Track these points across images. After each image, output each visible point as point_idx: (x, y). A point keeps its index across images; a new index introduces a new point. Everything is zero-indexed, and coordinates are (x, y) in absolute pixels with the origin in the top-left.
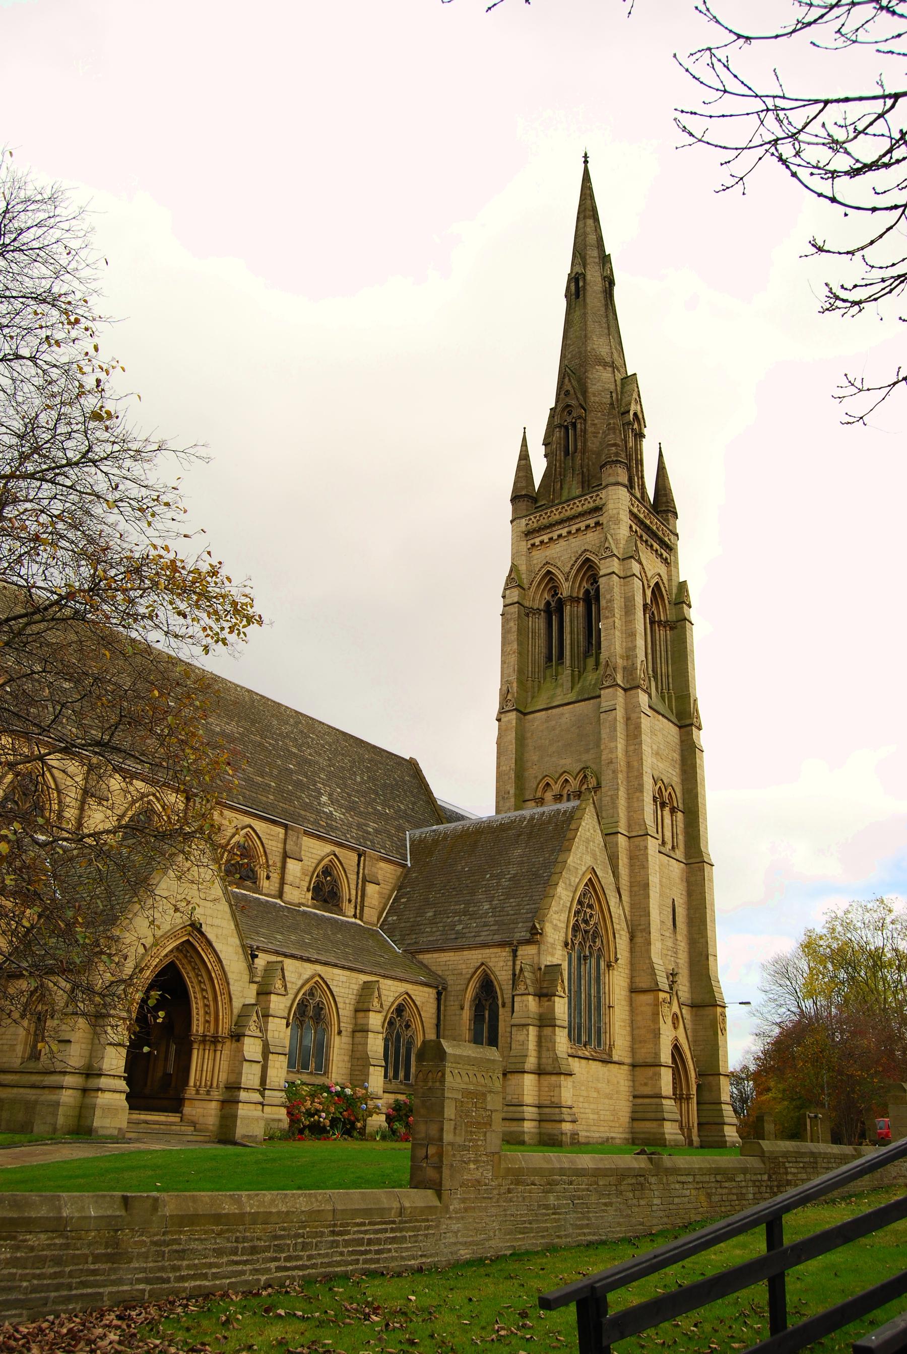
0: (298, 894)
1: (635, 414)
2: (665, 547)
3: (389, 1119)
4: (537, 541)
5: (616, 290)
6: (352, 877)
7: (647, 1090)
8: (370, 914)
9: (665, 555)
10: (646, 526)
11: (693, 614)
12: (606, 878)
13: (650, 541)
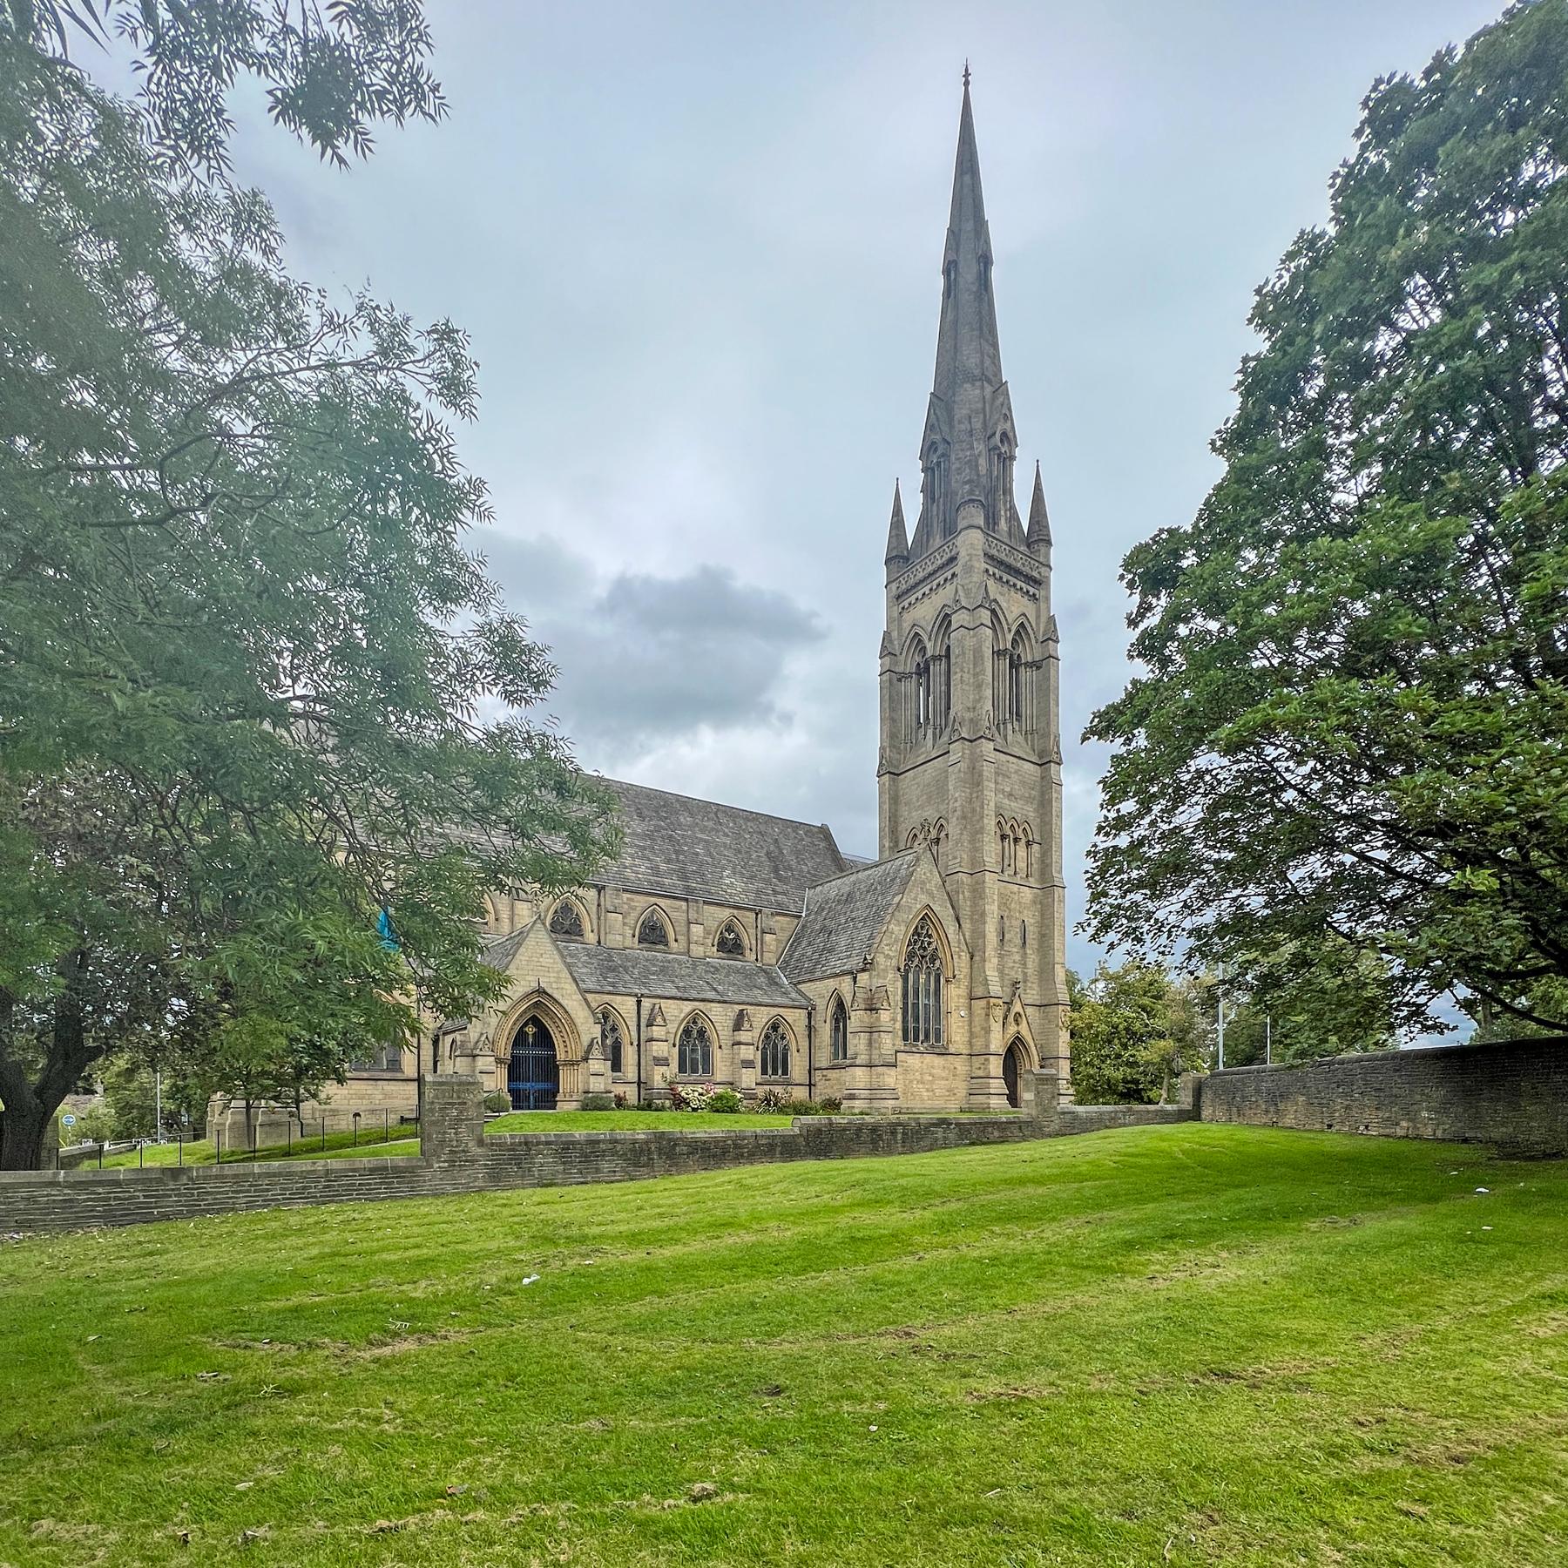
0: (705, 948)
1: (1004, 434)
2: (1034, 583)
3: (1450, 985)
4: (906, 604)
5: (995, 274)
6: (752, 931)
7: (980, 1073)
8: (769, 958)
9: (1032, 591)
10: (1001, 563)
11: (1061, 649)
12: (943, 911)
13: (1013, 580)
